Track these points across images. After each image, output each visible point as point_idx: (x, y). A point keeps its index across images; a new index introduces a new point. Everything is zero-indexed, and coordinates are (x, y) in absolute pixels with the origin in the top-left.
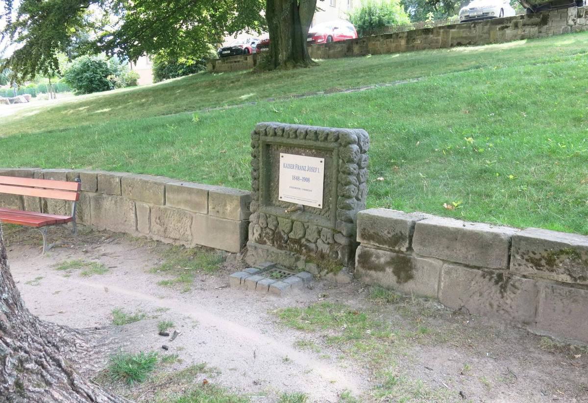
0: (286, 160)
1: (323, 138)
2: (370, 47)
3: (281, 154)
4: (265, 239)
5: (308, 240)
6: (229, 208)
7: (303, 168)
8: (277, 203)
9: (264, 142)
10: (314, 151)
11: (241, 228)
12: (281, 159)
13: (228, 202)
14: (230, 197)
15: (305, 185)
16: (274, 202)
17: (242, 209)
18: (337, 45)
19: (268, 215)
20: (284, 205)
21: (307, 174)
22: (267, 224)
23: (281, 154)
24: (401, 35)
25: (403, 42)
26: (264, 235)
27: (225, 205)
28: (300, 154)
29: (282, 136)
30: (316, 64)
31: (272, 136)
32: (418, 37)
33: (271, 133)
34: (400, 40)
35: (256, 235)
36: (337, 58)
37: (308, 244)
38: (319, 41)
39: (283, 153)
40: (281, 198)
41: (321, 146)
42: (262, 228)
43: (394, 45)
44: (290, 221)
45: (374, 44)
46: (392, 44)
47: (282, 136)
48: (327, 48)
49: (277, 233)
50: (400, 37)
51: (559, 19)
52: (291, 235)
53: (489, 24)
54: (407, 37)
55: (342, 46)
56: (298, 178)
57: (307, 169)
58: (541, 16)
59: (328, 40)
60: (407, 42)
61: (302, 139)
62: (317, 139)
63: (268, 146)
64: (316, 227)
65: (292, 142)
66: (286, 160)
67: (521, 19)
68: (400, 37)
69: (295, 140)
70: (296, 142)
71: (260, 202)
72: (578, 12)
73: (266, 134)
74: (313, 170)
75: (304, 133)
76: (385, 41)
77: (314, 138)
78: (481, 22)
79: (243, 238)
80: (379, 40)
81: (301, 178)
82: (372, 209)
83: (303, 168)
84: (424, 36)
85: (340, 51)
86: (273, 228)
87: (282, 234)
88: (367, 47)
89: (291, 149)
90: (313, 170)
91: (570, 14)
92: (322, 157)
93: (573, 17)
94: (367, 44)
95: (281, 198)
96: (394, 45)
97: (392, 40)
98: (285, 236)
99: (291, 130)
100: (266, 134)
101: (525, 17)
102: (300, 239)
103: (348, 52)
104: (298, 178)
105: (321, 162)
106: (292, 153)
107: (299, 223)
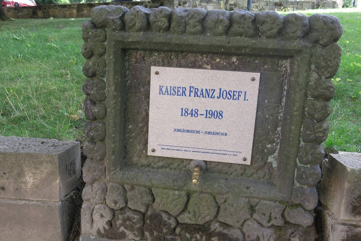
0: (164, 78)
1: (275, 31)
2: (51, 13)
3: (154, 69)
4: (122, 229)
5: (225, 225)
6: (30, 180)
7: (208, 94)
8: (144, 161)
9: (118, 42)
10: (234, 59)
11: (62, 215)
12: (153, 76)
13: (26, 169)
14: (34, 160)
15: (213, 124)
16: (135, 159)
17: (62, 179)
18: (25, 10)
19: (127, 187)
20: (160, 164)
21: (215, 105)
22: (126, 203)
23: (154, 69)
24: (72, 6)
25: (75, 11)
26: (119, 222)
27: (21, 174)
28: (200, 67)
29: (168, 29)
30: (12, 20)
31: (140, 30)
32: (85, 9)
33: (138, 25)
34: (72, 9)
35: (101, 224)
36: (26, 18)
37: (225, 231)
38: (8, 5)
39: (155, 65)
40: (245, 160)
41: (270, 46)
42: (113, 211)
43: (68, 13)
44: (184, 193)
45: (54, 11)
46: (67, 12)
47: (168, 29)
48: (16, 11)
49: (151, 218)
50: (72, 8)
51: (169, 5)
52: (186, 218)
53: (130, 4)
54: (77, 8)
55: (28, 11)
56: (194, 113)
57: (216, 94)
58: (160, 3)
59: (15, 5)
60: (78, 11)
61: (220, 34)
62: (257, 33)
63: (125, 51)
64: (247, 200)
65: (195, 42)
66: (164, 78)
67: (149, 3)
68: (72, 8)
69: (202, 37)
70: (203, 41)
71: (106, 162)
72: (179, 2)
73: (123, 27)
74: (232, 95)
75: (227, 22)
76: (61, 9)
77: (251, 32)
78: (125, 3)
79: (66, 230)
80: (57, 9)
81: (202, 111)
82: (333, 154)
83: (208, 94)
84: (89, 8)
85: (27, 14)
86: (143, 210)
87: (165, 217)
88: (48, 12)
89: (181, 54)
90: (232, 95)
91: (175, 3)
92: (254, 70)
93: (176, 5)
94: (48, 11)
95: (154, 151)
96: (68, 13)
97: (67, 9)
98: (172, 222)
99: (193, 17)
100: (123, 27)
101: (151, 2)
102: (209, 223)
103: (33, 15)
104: (194, 113)
105: (253, 80)
106: (180, 66)
107: (206, 195)
